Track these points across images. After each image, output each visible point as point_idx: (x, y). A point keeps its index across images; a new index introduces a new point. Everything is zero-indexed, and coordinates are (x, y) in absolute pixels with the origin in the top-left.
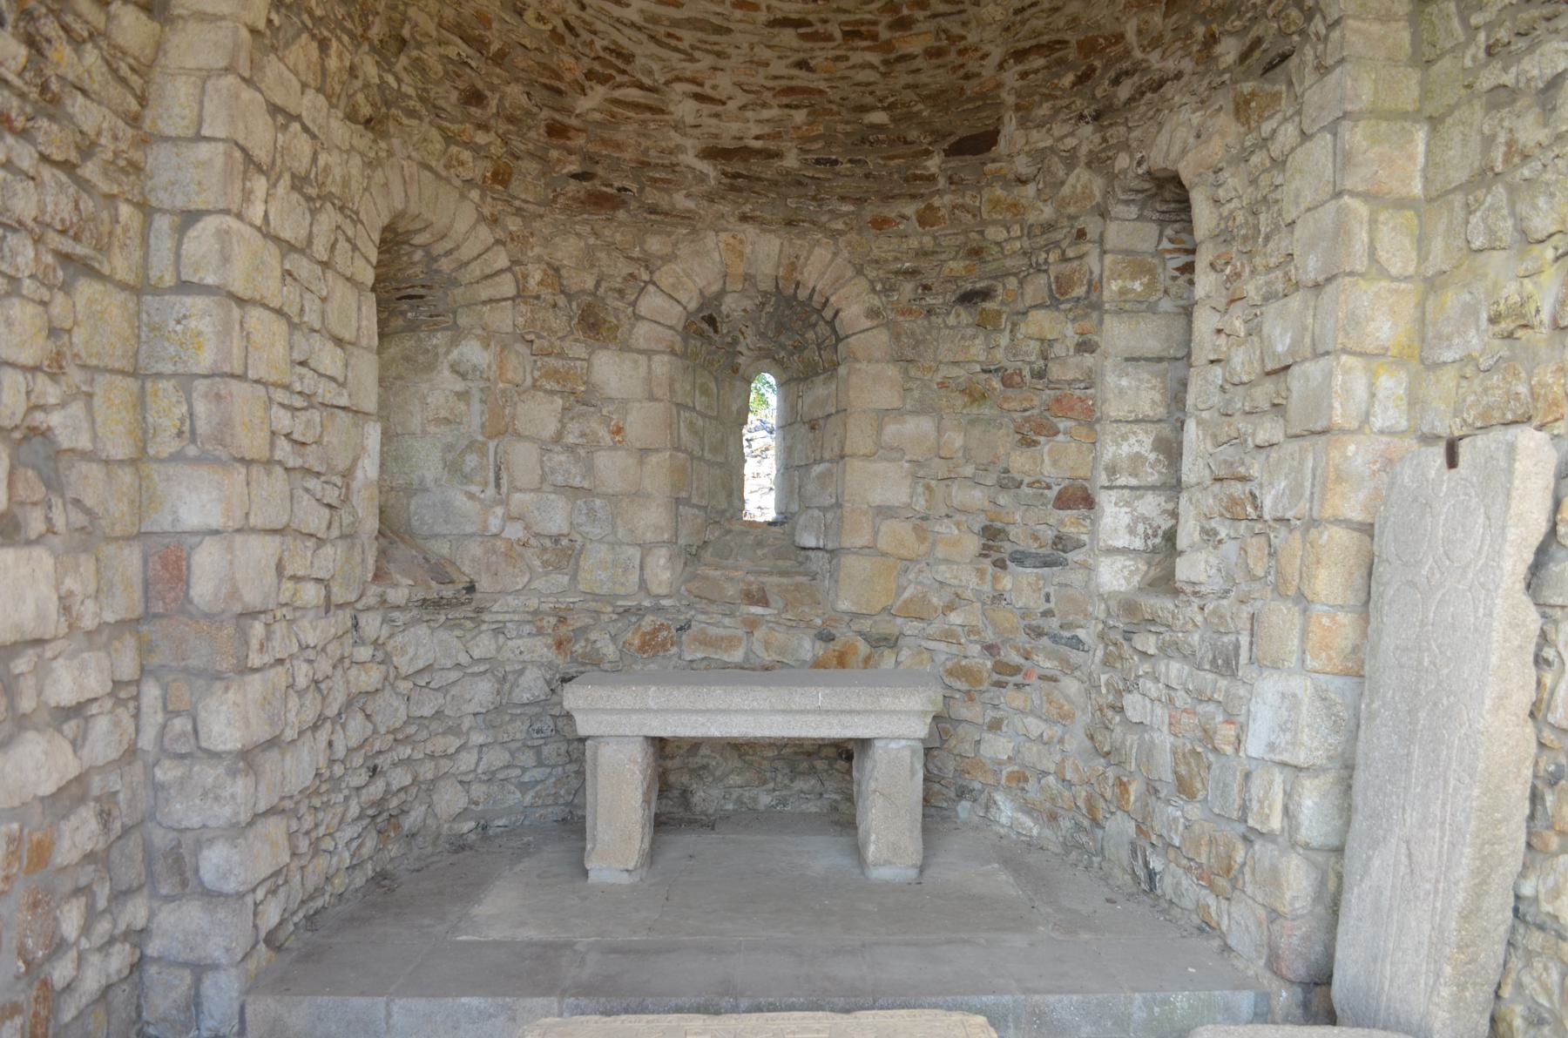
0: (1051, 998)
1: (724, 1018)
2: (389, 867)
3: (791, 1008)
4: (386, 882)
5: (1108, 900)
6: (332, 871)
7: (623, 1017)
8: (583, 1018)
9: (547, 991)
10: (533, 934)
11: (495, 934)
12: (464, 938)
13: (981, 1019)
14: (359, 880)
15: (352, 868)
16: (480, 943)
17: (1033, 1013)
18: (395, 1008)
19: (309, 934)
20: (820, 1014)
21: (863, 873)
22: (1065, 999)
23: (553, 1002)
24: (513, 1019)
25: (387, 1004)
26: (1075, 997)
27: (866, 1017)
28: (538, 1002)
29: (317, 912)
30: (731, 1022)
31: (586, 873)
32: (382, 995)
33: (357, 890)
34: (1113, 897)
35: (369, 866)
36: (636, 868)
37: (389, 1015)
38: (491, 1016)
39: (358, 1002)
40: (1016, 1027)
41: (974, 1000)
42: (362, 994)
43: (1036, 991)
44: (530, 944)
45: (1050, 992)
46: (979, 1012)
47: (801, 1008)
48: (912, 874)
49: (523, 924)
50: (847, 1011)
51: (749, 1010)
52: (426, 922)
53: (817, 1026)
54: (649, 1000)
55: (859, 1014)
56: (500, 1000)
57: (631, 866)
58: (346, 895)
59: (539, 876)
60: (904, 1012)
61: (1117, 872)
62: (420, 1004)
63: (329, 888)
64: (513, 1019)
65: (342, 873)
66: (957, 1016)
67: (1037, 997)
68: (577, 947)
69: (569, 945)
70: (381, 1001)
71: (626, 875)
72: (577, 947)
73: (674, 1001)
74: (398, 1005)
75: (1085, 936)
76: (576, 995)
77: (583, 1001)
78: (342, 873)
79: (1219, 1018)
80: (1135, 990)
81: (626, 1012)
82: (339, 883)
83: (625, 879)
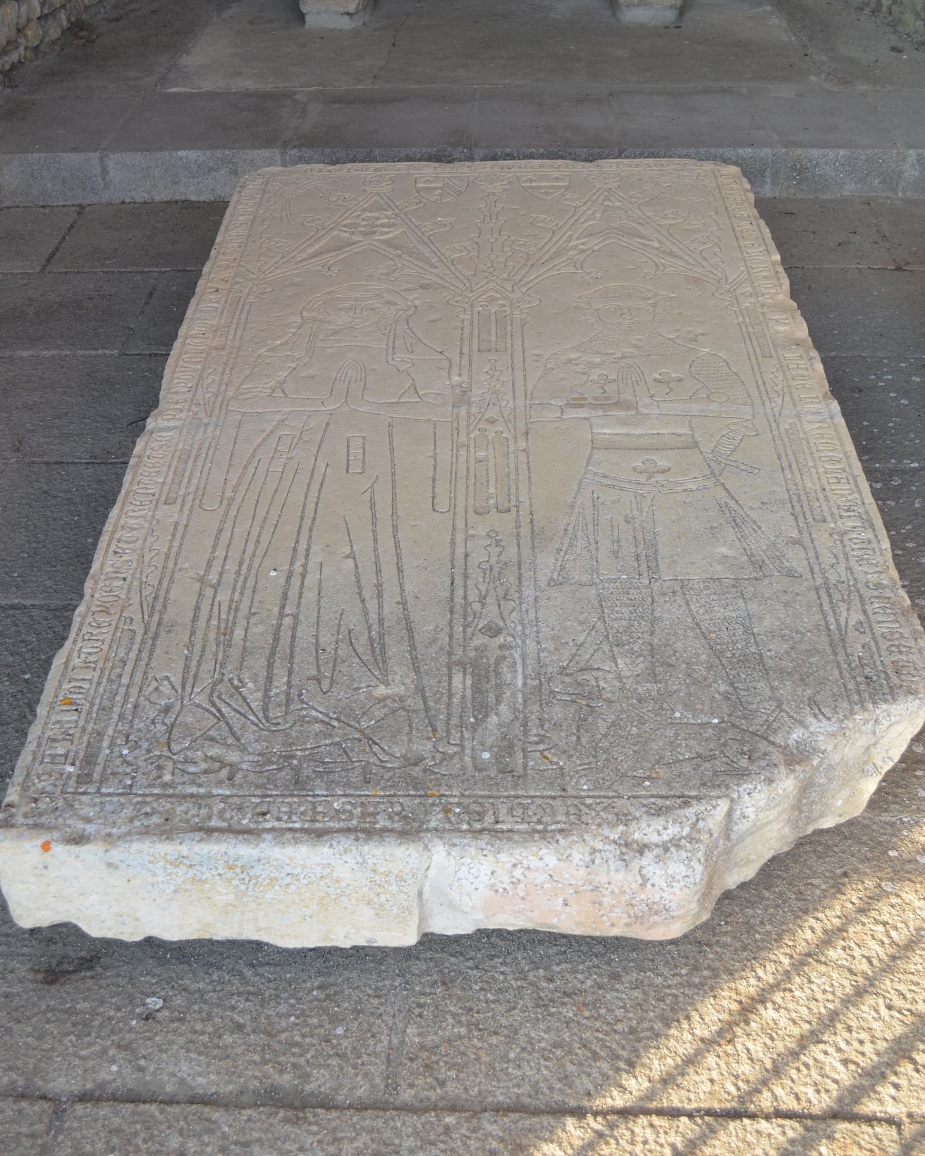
0: (815, 153)
1: (456, 165)
2: (85, 16)
3: (531, 157)
4: (84, 33)
5: (894, 49)
6: (23, 21)
7: (350, 165)
8: (307, 167)
9: (268, 143)
10: (249, 84)
11: (208, 85)
12: (174, 90)
13: (734, 170)
14: (54, 32)
15: (43, 18)
16: (192, 94)
17: (794, 168)
18: (110, 165)
19: (10, 90)
20: (560, 162)
21: (614, 15)
22: (831, 154)
23: (276, 153)
24: (235, 172)
25: (101, 160)
26: (842, 152)
27: (610, 166)
28: (265, 153)
29: (13, 67)
30: (463, 169)
31: (301, 17)
32: (95, 151)
33: (53, 43)
34: (900, 45)
35: (63, 16)
36: (357, 12)
37: (105, 171)
38: (211, 170)
39: (72, 158)
40: (773, 183)
41: (730, 153)
42: (74, 150)
43: (799, 145)
44: (247, 95)
45: (814, 146)
46: (735, 164)
47: (541, 157)
48: (670, 16)
49: (238, 74)
50: (589, 159)
51: (485, 159)
52: (132, 74)
53: (556, 174)
54: (377, 151)
55: (601, 162)
56: (219, 153)
57: (352, 8)
58: (42, 48)
59: (251, 22)
60: (651, 161)
61: (909, 17)
62: (136, 159)
63: (22, 41)
64: (235, 172)
65: (34, 23)
66: (708, 166)
67: (799, 151)
68: (297, 97)
69: (288, 95)
70: (94, 157)
71: (346, 19)
72: (297, 97)
73: (404, 152)
74: (114, 161)
75: (862, 87)
76: (300, 146)
77: (307, 153)
78: (34, 23)
79: (884, 784)
80: (910, 146)
81: (353, 161)
82: (33, 35)
83: (346, 24)
